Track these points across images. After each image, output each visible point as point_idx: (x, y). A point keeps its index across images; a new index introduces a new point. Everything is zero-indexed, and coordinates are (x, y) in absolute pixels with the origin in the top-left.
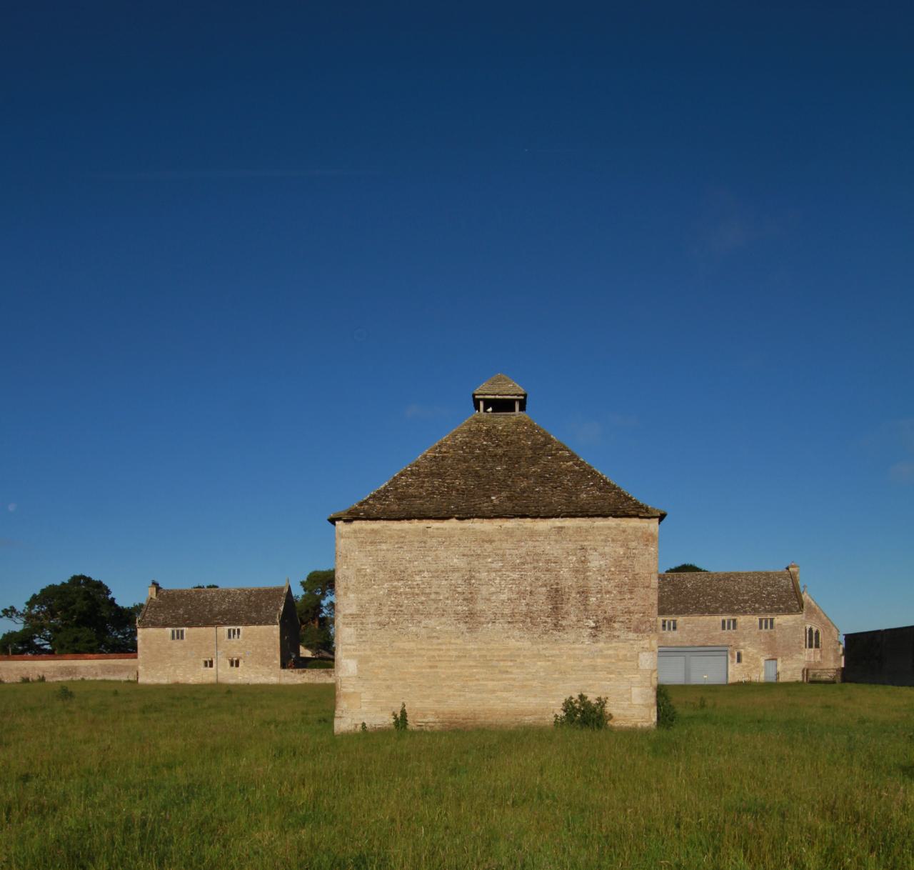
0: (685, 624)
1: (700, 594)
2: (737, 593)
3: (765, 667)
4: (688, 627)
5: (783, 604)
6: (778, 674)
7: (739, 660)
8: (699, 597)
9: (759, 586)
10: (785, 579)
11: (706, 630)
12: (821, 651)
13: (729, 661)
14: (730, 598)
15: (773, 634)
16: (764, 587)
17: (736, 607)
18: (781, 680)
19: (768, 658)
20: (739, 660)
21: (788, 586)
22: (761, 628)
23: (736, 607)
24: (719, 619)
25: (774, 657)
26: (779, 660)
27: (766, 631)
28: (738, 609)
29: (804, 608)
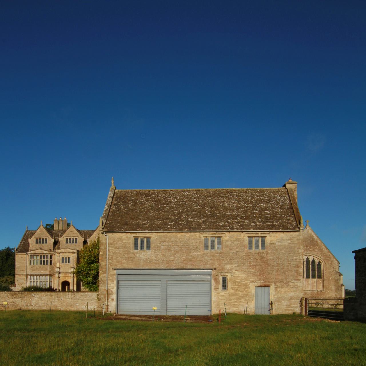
0: (161, 242)
1: (184, 209)
2: (226, 209)
3: (256, 295)
4: (164, 246)
5: (277, 220)
6: (271, 304)
7: (225, 286)
8: (182, 212)
9: (252, 203)
10: (281, 195)
11: (184, 249)
12: (323, 281)
13: (213, 288)
14: (216, 214)
15: (265, 255)
16: (257, 203)
17: (222, 223)
18: (275, 312)
19: (259, 284)
20: (225, 286)
21: (284, 202)
22: (251, 247)
23: (222, 223)
24: (201, 236)
25: (267, 284)
26: (273, 287)
27: (257, 251)
28: (224, 226)
29: (302, 225)
